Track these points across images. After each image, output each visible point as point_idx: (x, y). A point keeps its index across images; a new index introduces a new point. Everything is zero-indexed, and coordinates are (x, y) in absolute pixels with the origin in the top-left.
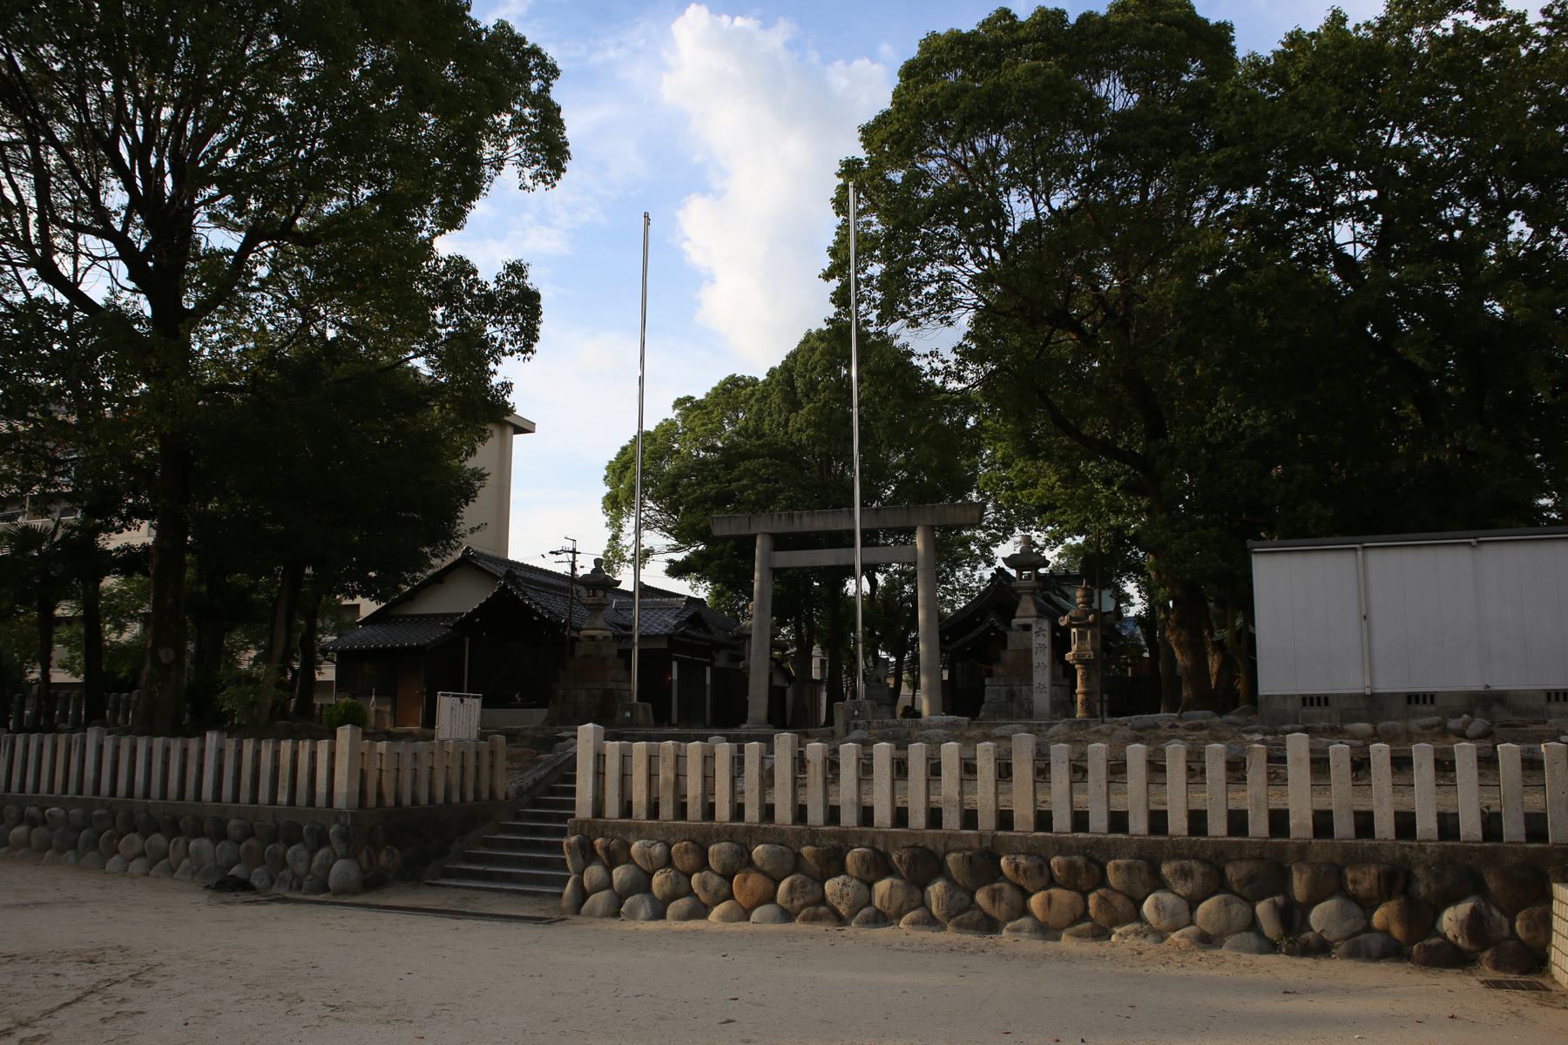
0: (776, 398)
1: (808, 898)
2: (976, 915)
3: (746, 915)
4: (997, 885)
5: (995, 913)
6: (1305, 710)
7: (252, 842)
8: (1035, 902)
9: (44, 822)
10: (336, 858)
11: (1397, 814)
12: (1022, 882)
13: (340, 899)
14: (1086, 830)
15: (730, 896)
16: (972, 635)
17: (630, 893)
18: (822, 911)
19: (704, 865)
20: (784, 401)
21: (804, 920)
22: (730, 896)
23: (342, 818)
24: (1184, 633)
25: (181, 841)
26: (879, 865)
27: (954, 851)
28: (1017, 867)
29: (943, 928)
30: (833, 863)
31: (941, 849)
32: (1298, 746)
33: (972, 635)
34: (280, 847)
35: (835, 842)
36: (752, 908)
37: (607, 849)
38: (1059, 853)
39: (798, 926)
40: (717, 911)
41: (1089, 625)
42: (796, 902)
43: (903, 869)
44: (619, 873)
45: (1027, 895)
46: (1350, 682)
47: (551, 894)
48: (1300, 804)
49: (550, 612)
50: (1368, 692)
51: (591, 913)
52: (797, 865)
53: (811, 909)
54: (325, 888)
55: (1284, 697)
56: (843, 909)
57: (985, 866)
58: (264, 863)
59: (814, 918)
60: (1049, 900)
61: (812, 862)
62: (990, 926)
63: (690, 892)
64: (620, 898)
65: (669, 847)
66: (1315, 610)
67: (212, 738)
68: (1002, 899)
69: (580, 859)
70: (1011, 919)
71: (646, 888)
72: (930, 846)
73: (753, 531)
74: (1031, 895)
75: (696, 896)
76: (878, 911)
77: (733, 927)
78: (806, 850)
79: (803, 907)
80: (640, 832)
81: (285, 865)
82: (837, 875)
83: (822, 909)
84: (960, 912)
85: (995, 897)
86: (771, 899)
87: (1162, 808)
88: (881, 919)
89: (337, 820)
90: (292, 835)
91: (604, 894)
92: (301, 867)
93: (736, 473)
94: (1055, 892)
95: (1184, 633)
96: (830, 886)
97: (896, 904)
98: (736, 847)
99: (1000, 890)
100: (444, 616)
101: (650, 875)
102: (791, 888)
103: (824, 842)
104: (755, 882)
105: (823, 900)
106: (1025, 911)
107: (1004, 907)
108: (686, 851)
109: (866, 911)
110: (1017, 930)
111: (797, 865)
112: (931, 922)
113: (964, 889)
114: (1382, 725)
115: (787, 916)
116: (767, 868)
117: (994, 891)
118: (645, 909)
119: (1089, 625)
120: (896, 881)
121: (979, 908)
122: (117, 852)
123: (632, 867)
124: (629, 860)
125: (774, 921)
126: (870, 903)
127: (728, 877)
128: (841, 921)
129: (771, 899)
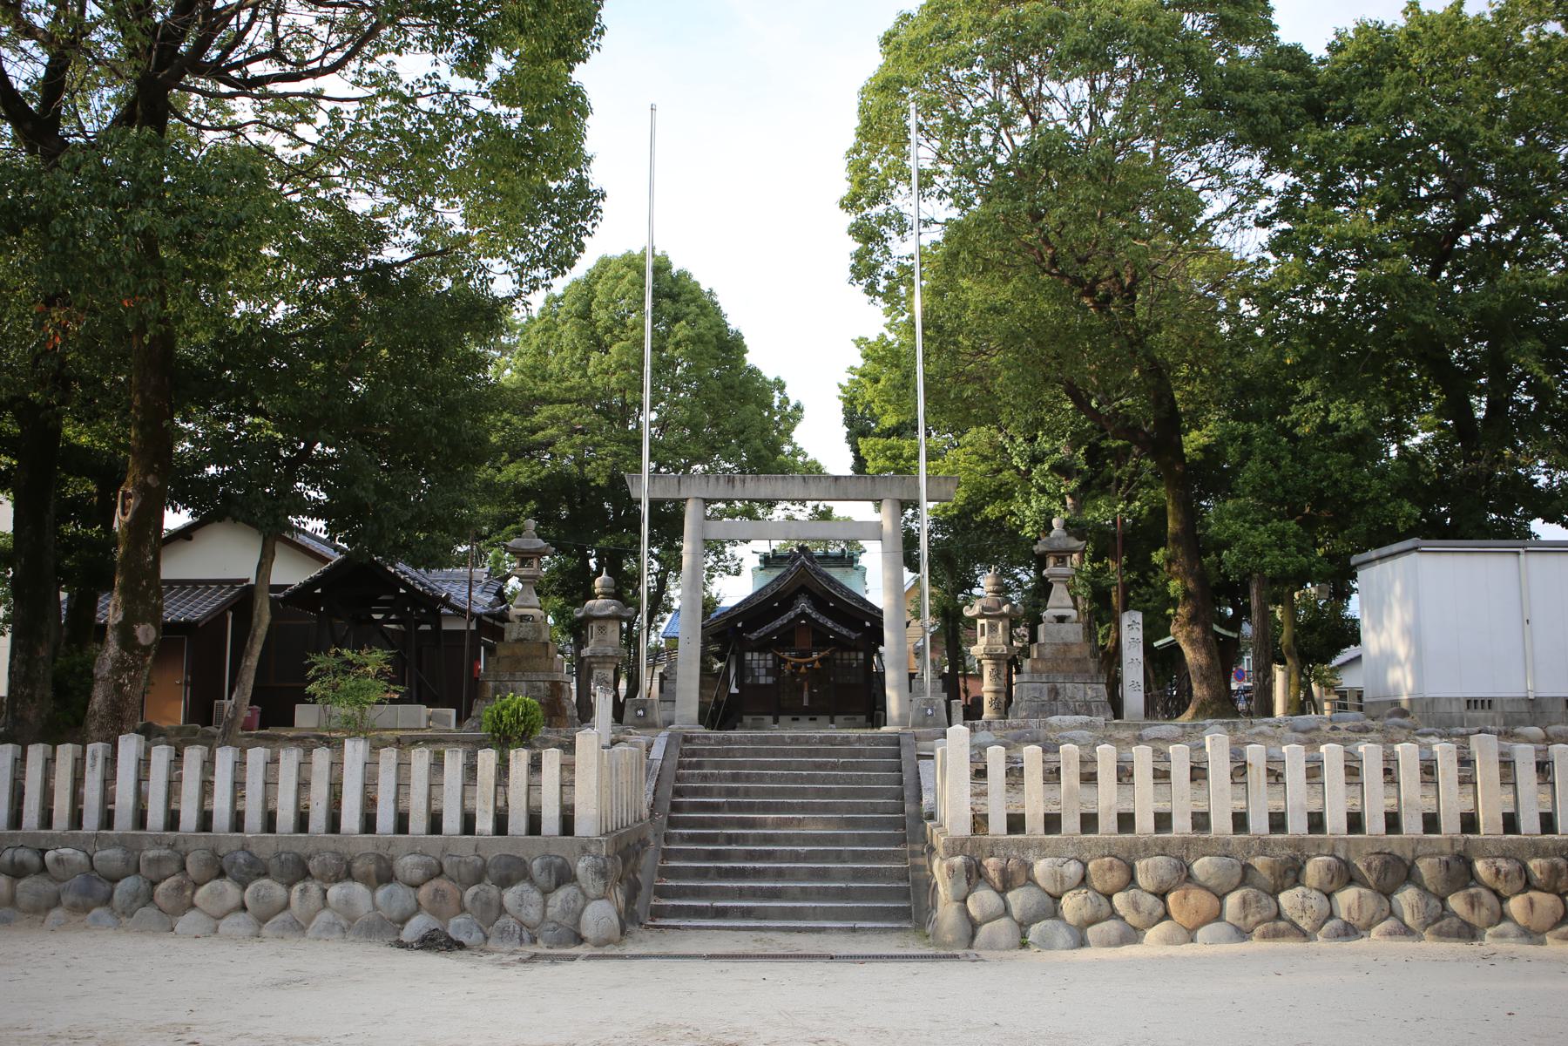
0: (568, 332)
1: (1266, 914)
2: (1455, 923)
3: (1190, 935)
4: (1472, 891)
5: (1474, 919)
6: (1470, 714)
7: (442, 884)
8: (1515, 905)
9: (43, 868)
10: (587, 899)
11: (1386, 814)
12: (1500, 886)
13: (608, 950)
14: (1554, 832)
15: (1167, 915)
16: (778, 623)
17: (1036, 919)
18: (1280, 927)
19: (1131, 881)
20: (580, 335)
21: (1264, 936)
22: (1167, 915)
23: (593, 849)
24: (1197, 630)
25: (314, 888)
26: (1346, 875)
27: (1425, 856)
28: (1498, 872)
29: (1421, 938)
30: (1292, 873)
31: (1409, 855)
32: (1485, 749)
33: (778, 623)
34: (494, 891)
35: (1289, 852)
36: (1196, 928)
37: (1003, 871)
38: (1536, 855)
39: (1255, 945)
40: (1152, 934)
41: (1002, 617)
42: (1251, 919)
43: (1371, 878)
44: (1018, 899)
45: (1502, 899)
46: (1509, 685)
47: (840, 929)
48: (1491, 805)
49: (422, 584)
50: (1531, 696)
51: (991, 945)
52: (1246, 875)
53: (1271, 925)
54: (580, 940)
55: (1450, 700)
56: (1305, 923)
57: (1460, 872)
58: (463, 910)
59: (1276, 935)
60: (1531, 903)
61: (1266, 874)
62: (1469, 932)
63: (1113, 914)
64: (1023, 926)
65: (1085, 866)
66: (1418, 614)
67: (129, 746)
68: (1481, 904)
69: (964, 883)
70: (1490, 925)
71: (1056, 914)
72: (1398, 853)
73: (683, 495)
74: (1508, 898)
75: (1123, 918)
76: (1346, 924)
77: (1173, 950)
78: (1259, 862)
79: (1258, 923)
80: (1147, 849)
81: (502, 910)
82: (1292, 886)
83: (1281, 925)
84: (1436, 920)
85: (1473, 902)
86: (1219, 917)
87: (1020, 811)
88: (1349, 931)
89: (584, 850)
90: (512, 872)
91: (1004, 921)
92: (533, 914)
93: (537, 419)
94: (1532, 894)
95: (1197, 630)
96: (1285, 898)
97: (1366, 915)
98: (1174, 861)
99: (1477, 895)
100: (220, 583)
101: (1056, 898)
102: (1244, 903)
103: (1277, 851)
104: (1199, 900)
105: (1279, 916)
106: (1503, 916)
107: (1484, 912)
108: (1111, 868)
109: (1332, 924)
110: (1502, 936)
111: (1246, 875)
112: (1407, 931)
113: (1436, 895)
114: (1552, 729)
115: (1243, 934)
116: (1211, 883)
117: (1472, 896)
118: (1063, 936)
119: (1002, 617)
120: (1363, 890)
121: (1454, 914)
122: (193, 906)
123: (1034, 890)
124: (1031, 881)
125: (1230, 940)
126: (1331, 915)
127: (1162, 896)
128: (1305, 935)
129: (1219, 917)
